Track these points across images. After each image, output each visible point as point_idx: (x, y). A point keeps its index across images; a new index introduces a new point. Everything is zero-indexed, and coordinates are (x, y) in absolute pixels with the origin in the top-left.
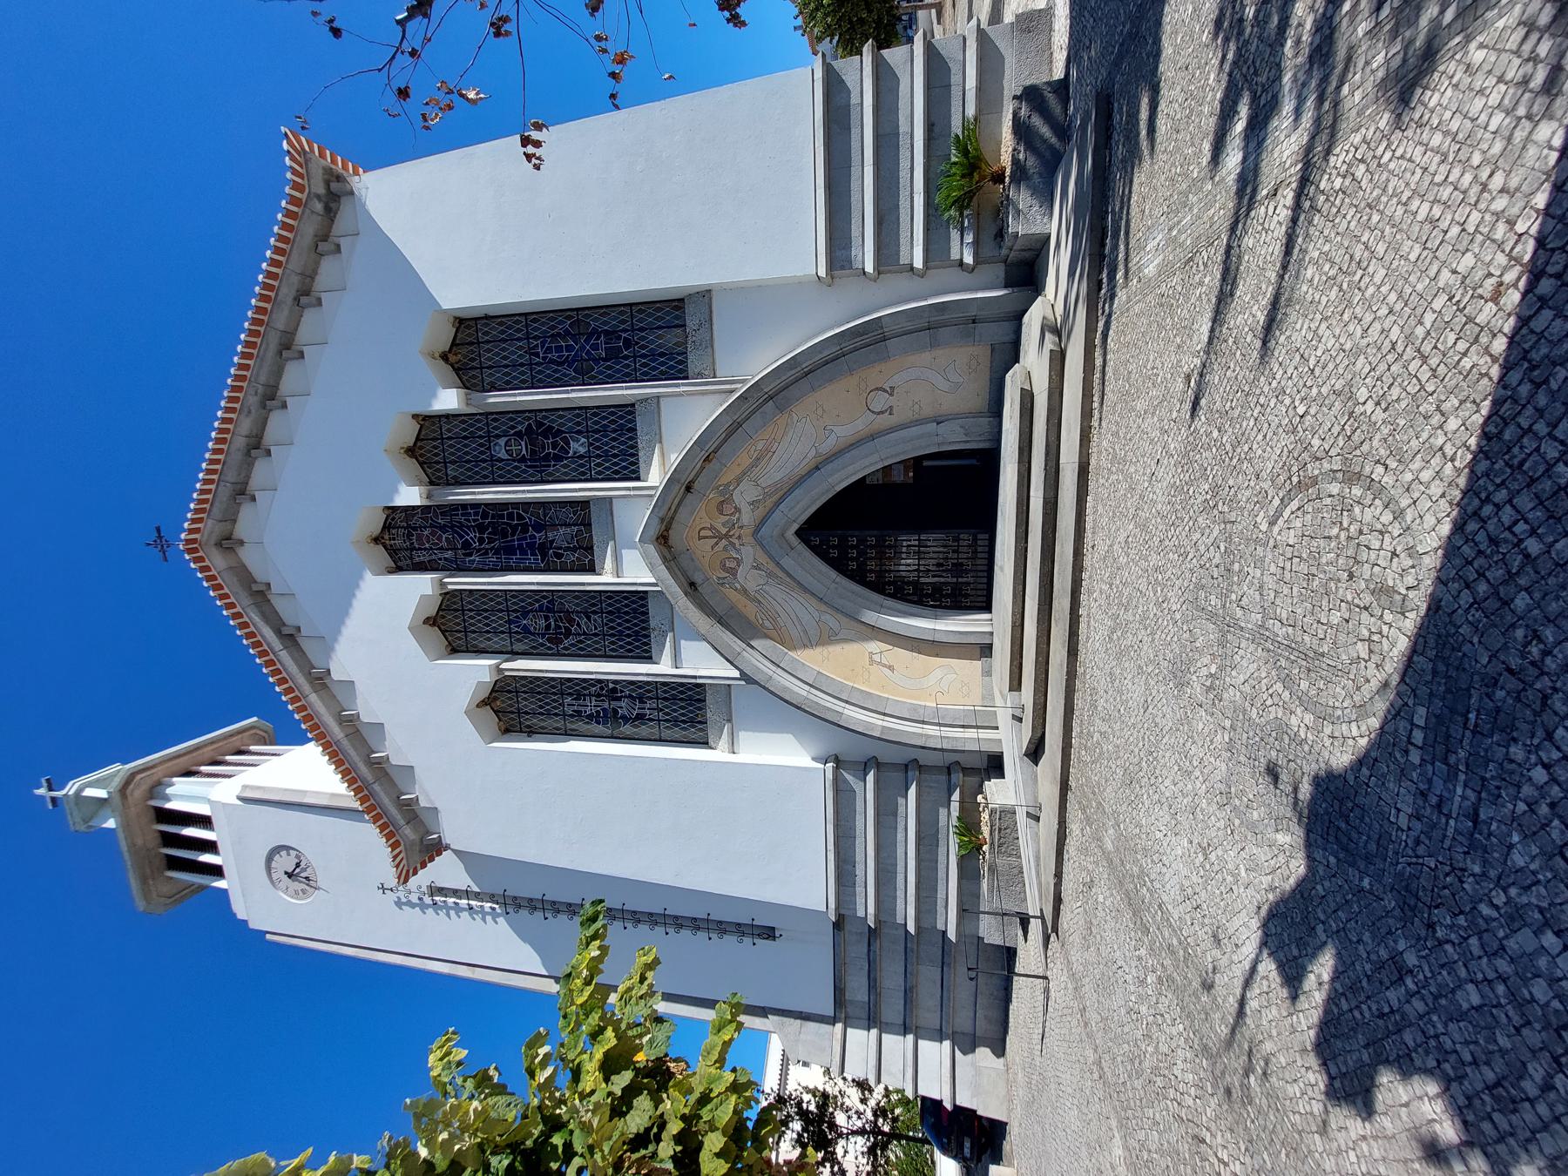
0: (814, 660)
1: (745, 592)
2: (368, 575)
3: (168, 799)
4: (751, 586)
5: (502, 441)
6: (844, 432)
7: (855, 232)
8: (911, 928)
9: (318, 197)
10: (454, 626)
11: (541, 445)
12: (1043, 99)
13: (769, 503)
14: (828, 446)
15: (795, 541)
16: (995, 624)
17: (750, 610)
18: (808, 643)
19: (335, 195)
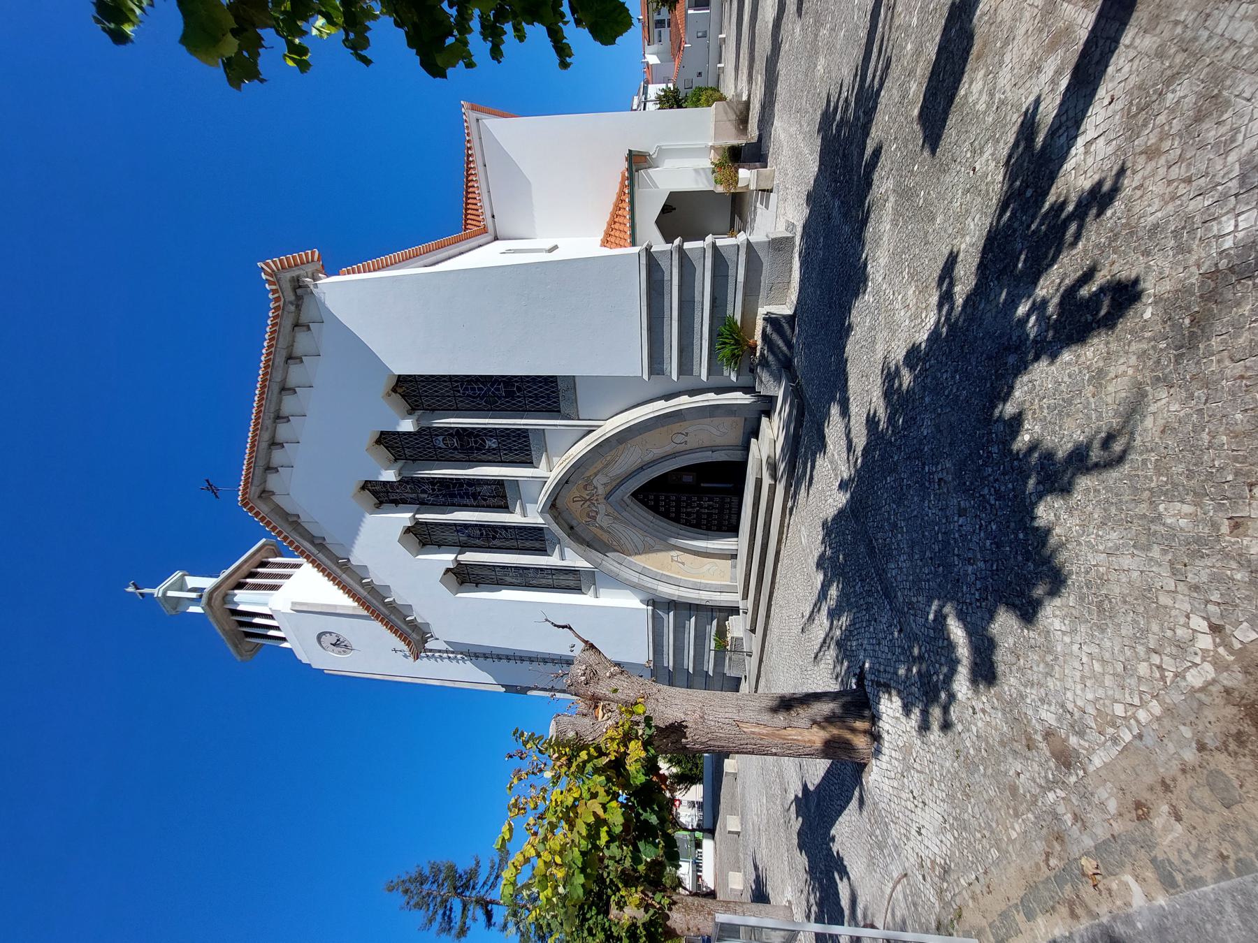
0: (640, 561)
1: (601, 528)
2: (367, 515)
3: (237, 604)
4: (605, 525)
5: (441, 438)
6: (657, 452)
7: (666, 355)
8: (691, 671)
9: (291, 303)
10: (423, 537)
11: (470, 446)
12: (781, 326)
13: (614, 484)
14: (647, 458)
15: (629, 501)
16: (739, 544)
17: (605, 537)
18: (638, 553)
19: (300, 291)
